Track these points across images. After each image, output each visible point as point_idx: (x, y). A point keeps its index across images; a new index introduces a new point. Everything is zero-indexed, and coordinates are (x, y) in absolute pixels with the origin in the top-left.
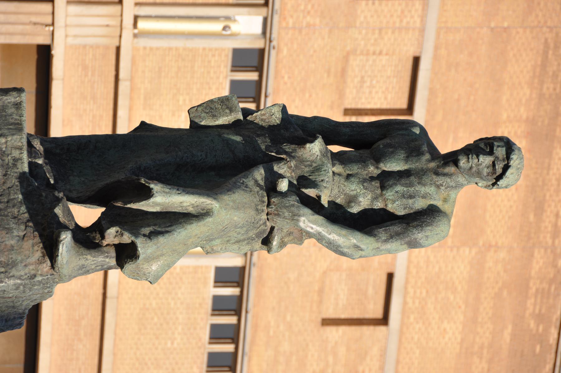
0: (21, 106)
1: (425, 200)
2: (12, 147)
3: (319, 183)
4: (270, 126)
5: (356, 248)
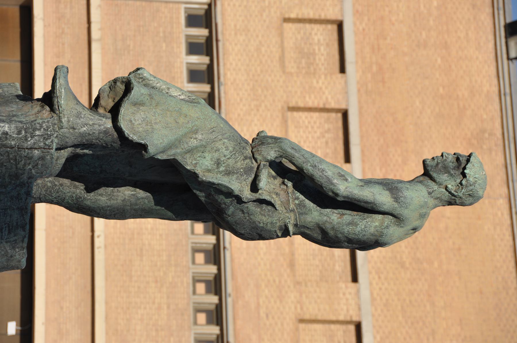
5: (340, 176)
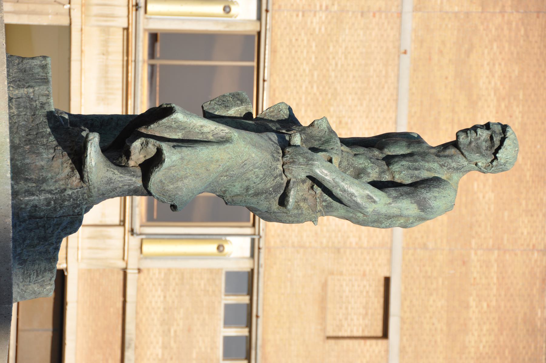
1: (429, 172)
5: (369, 199)
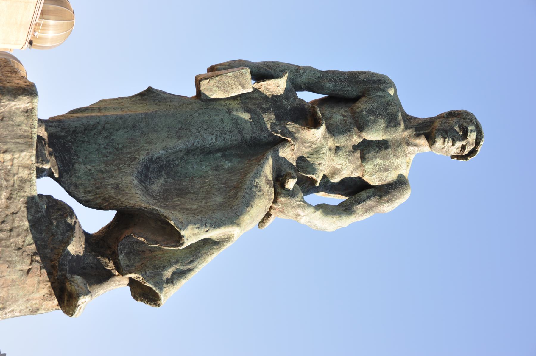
0: (33, 115)
2: (19, 166)
3: (316, 167)
4: (273, 95)
